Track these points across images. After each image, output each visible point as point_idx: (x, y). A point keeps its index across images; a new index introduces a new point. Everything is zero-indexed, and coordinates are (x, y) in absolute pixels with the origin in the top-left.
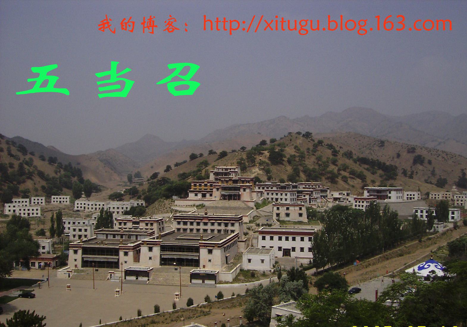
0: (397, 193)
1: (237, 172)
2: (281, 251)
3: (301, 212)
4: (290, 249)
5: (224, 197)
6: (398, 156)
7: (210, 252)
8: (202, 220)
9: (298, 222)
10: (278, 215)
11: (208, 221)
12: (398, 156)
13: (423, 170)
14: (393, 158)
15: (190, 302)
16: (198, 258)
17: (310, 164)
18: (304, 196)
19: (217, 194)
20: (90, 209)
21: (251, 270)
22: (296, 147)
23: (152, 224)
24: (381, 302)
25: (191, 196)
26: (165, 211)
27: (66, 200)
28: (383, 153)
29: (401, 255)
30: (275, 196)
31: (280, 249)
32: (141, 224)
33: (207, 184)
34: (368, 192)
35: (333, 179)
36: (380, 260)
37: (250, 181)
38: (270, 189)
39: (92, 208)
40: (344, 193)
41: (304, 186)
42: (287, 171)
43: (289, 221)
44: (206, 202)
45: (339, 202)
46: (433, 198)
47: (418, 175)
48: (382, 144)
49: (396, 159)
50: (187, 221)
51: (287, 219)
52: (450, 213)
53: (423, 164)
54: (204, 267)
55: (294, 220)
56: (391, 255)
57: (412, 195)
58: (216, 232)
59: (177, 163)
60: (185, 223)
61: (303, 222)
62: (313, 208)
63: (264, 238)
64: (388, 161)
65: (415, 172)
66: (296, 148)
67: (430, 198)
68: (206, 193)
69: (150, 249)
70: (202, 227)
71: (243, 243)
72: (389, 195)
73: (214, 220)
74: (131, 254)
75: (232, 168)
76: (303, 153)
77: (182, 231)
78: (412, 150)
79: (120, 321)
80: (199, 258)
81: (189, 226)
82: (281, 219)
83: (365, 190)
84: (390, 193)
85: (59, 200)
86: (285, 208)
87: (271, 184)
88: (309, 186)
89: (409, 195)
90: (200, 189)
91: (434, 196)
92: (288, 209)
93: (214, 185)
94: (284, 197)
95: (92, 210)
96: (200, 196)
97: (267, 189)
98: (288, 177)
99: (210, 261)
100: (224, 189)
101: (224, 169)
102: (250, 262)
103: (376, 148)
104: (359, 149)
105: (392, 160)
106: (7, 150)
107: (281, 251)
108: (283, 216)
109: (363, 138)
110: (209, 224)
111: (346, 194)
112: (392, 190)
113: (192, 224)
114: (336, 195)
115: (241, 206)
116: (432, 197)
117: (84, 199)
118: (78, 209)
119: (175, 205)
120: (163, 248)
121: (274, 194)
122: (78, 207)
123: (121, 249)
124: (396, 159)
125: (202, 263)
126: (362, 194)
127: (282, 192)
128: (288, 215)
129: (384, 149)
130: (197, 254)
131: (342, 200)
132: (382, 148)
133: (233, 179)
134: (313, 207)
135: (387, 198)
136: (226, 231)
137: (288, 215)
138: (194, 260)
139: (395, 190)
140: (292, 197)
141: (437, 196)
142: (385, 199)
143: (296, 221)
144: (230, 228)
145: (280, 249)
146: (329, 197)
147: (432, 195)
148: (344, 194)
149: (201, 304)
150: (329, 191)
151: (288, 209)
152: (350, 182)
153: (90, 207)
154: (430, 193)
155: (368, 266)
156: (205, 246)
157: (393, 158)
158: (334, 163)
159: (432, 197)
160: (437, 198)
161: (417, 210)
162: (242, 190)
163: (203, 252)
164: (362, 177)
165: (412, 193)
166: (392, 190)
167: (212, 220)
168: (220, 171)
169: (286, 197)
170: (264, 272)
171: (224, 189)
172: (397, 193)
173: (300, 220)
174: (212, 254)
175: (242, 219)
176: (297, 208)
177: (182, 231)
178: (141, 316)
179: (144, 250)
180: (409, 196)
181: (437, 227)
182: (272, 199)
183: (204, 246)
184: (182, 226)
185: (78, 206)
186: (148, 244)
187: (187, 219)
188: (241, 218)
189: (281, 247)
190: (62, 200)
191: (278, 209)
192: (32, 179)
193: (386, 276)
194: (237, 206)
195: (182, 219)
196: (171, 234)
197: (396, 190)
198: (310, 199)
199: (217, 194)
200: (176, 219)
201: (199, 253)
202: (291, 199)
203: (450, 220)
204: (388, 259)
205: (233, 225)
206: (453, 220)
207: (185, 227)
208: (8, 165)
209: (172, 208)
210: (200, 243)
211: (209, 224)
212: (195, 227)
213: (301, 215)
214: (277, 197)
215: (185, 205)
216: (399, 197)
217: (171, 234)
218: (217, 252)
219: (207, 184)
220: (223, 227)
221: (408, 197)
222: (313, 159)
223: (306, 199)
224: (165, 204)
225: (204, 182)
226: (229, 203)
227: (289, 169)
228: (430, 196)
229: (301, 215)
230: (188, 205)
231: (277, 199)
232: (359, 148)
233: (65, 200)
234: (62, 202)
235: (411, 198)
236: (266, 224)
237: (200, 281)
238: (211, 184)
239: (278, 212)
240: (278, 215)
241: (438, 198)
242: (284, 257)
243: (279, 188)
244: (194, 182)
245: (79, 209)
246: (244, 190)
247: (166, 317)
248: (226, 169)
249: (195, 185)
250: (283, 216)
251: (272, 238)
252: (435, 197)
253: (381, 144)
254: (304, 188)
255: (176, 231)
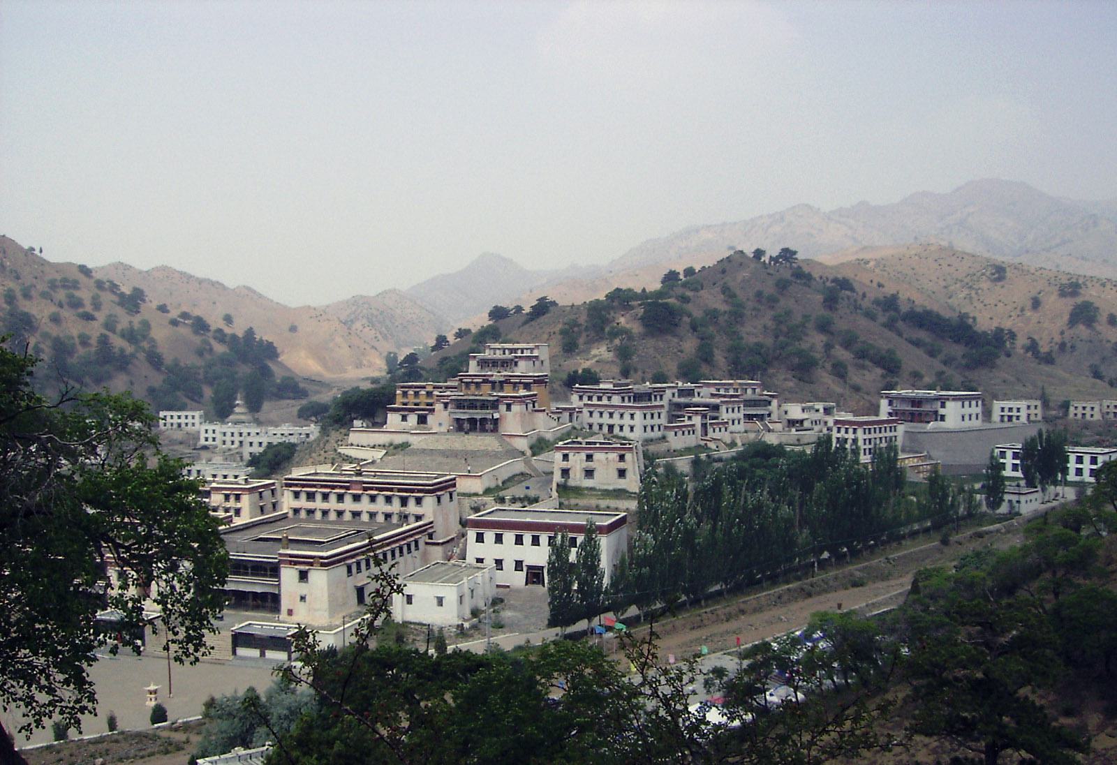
0: (963, 407)
1: (536, 357)
2: (522, 570)
3: (622, 465)
4: (543, 567)
5: (459, 426)
6: (1036, 304)
7: (303, 576)
8: (348, 488)
9: (615, 490)
10: (565, 472)
11: (361, 492)
12: (1036, 304)
13: (1091, 341)
14: (1022, 310)
15: (159, 714)
16: (277, 592)
17: (755, 331)
18: (690, 418)
19: (441, 419)
20: (228, 445)
21: (411, 623)
22: (726, 290)
23: (238, 498)
25: (393, 419)
26: (322, 458)
27: (193, 421)
28: (1000, 298)
29: (856, 584)
30: (606, 420)
31: (519, 565)
33: (432, 392)
34: (890, 404)
35: (804, 369)
36: (785, 598)
37: (531, 383)
38: (605, 401)
39: (233, 443)
40: (817, 407)
41: (713, 390)
42: (682, 351)
43: (592, 489)
44: (415, 437)
45: (797, 431)
46: (1079, 416)
47: (1075, 354)
48: (999, 273)
49: (1028, 314)
50: (314, 490)
51: (588, 483)
52: (1072, 458)
53: (1094, 324)
54: (290, 612)
55: (605, 487)
56: (827, 583)
57: (1015, 410)
58: (365, 517)
59: (460, 329)
60: (311, 496)
61: (627, 492)
62: (710, 449)
63: (480, 538)
64: (1010, 316)
65: (1069, 345)
66: (726, 294)
67: (1071, 415)
68: (427, 414)
70: (348, 505)
71: (439, 549)
72: (942, 411)
73: (377, 489)
75: (527, 349)
76: (741, 306)
77: (303, 514)
78: (1071, 288)
79: (110, 733)
80: (280, 591)
81: (319, 504)
82: (571, 483)
83: (882, 397)
84: (943, 406)
85: (176, 420)
86: (583, 455)
87: (611, 386)
88: (727, 390)
89: (1006, 410)
90: (415, 404)
91: (1080, 411)
92: (589, 457)
93: (438, 396)
94: (627, 421)
95: (233, 446)
96: (413, 419)
97: (589, 402)
98: (680, 367)
99: (303, 598)
100: (460, 404)
101: (507, 352)
102: (411, 603)
103: (985, 285)
104: (945, 287)
105: (1018, 316)
106: (91, 304)
107: (522, 570)
108: (578, 476)
109: (960, 259)
110: (365, 499)
111: (822, 410)
112: (948, 399)
113: (325, 497)
114: (795, 411)
115: (490, 449)
116: (1076, 415)
117: (243, 417)
118: (207, 443)
119: (349, 442)
121: (606, 415)
122: (207, 439)
124: (1028, 314)
125: (285, 604)
126: (875, 410)
127: (622, 411)
128: (589, 473)
129: (1003, 287)
130: (273, 581)
131: (806, 424)
132: (1000, 284)
134: (712, 445)
135: (936, 420)
136: (404, 518)
137: (589, 473)
138: (269, 596)
139: (955, 398)
140: (649, 422)
141: (1088, 412)
142: (929, 422)
143: (611, 488)
144: (412, 508)
145: (519, 565)
146: (774, 417)
147: (1076, 408)
148: (817, 411)
149: (180, 721)
150: (775, 403)
151: (589, 457)
152: (855, 377)
153: (228, 438)
154: (1072, 403)
155: (737, 616)
156: (293, 561)
157: (1022, 310)
158: (824, 327)
159: (1076, 415)
160: (1088, 417)
161: (1005, 452)
162: (503, 408)
163: (288, 575)
164: (890, 367)
165: (1014, 404)
166: (948, 398)
167: (371, 489)
168: (499, 355)
169: (632, 423)
171: (460, 404)
172: (963, 407)
173: (620, 487)
175: (454, 485)
176: (614, 456)
177: (303, 514)
178: (166, 721)
180: (1006, 413)
181: (1018, 502)
182: (601, 426)
183: (290, 562)
184: (303, 503)
185: (207, 435)
187: (314, 486)
188: (451, 484)
189: (521, 562)
190: (183, 421)
191: (566, 457)
192: (128, 373)
193: (729, 654)
194: (482, 448)
195: (303, 486)
196: (271, 522)
197: (959, 399)
198: (704, 426)
199: (441, 419)
200: (291, 485)
201: (279, 578)
202: (645, 427)
203: (1072, 477)
204: (809, 595)
205: (419, 501)
206: (1078, 479)
207: (310, 505)
208: (77, 341)
209: (339, 451)
210: (281, 555)
211: (365, 499)
212: (333, 504)
213: (622, 473)
214: (611, 422)
215: (372, 445)
216: (970, 415)
217: (271, 522)
218: (319, 577)
219: (432, 392)
220: (396, 507)
221: (1003, 414)
222: (767, 319)
223: (693, 425)
224: (328, 441)
225: (424, 387)
226: (462, 441)
227: (690, 345)
228: (1072, 409)
229: (622, 473)
230: (377, 443)
231: (611, 427)
232: (943, 284)
233: (190, 420)
234: (183, 426)
235: (1010, 418)
236: (522, 496)
237: (255, 653)
238: (415, 392)
239: (565, 465)
240: (565, 472)
241: (1092, 416)
242: (530, 586)
243: (629, 398)
244: (402, 387)
245: (210, 442)
246: (509, 407)
247: (61, 755)
248: (512, 351)
249: (405, 394)
250: (578, 476)
251: (499, 539)
252: (1084, 414)
253: (996, 276)
254: (713, 395)
255: (291, 514)
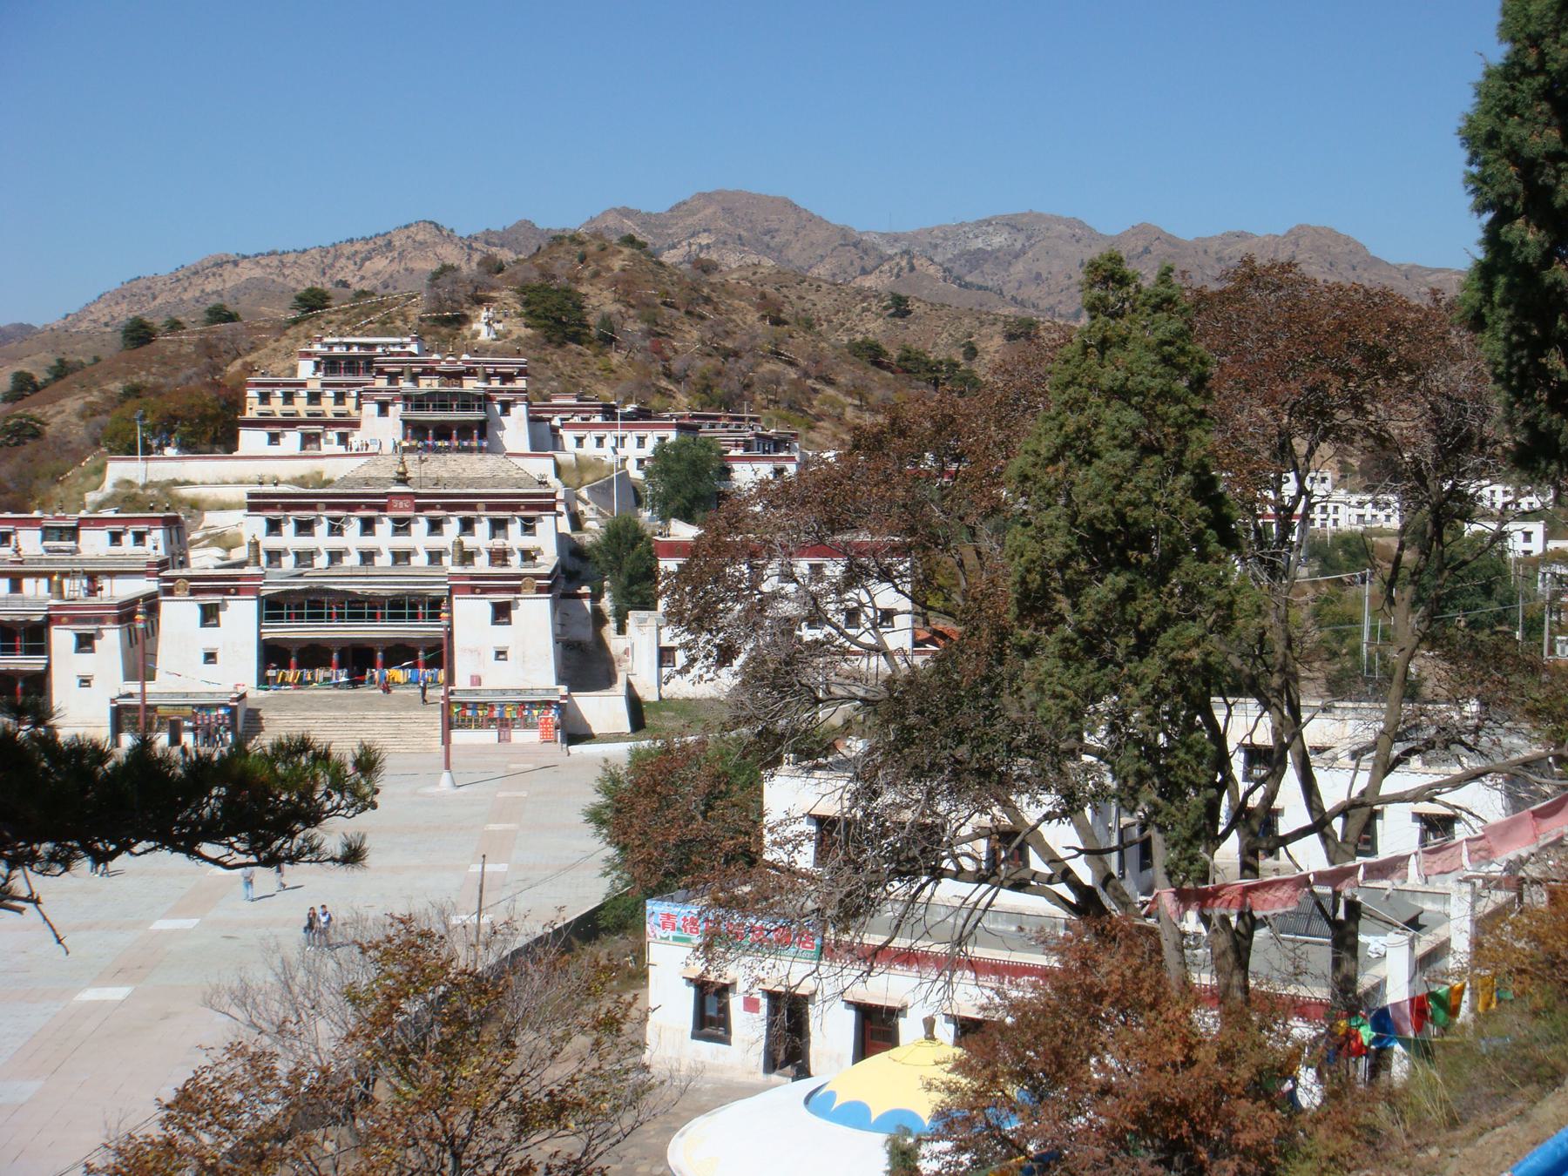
24: (1023, 1128)
25: (251, 440)
32: (86, 535)
69: (210, 615)
73: (445, 507)
74: (111, 639)
87: (574, 402)
99: (501, 654)
100: (417, 402)
120: (273, 608)
123: (57, 620)
133: (439, 368)
156: (476, 587)
170: (1472, 192)
174: (509, 623)
179: (179, 615)
183: (473, 590)
186: (194, 592)
195: (288, 507)
212: (352, 538)
